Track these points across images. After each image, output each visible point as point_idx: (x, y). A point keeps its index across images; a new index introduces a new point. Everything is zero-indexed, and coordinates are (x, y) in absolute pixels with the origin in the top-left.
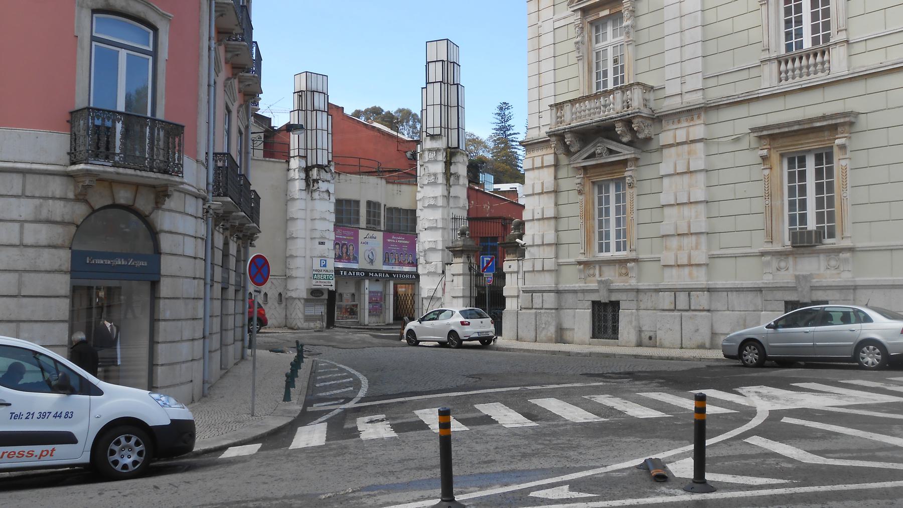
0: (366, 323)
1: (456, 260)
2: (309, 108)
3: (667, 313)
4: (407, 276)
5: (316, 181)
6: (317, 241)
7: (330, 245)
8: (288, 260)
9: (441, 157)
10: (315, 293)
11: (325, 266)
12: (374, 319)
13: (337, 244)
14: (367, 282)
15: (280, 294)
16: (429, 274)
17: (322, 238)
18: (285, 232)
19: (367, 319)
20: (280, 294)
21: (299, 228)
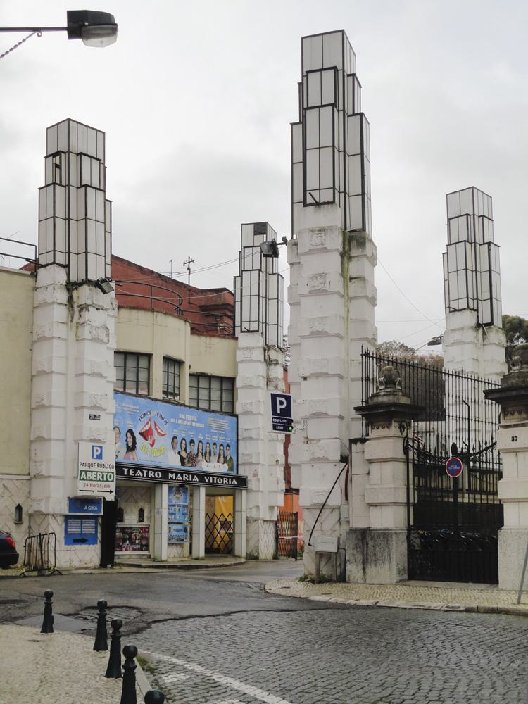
0: (164, 558)
1: (374, 433)
2: (73, 182)
3: (243, 609)
4: (225, 481)
5: (83, 308)
6: (87, 413)
7: (107, 422)
8: (34, 446)
9: (336, 242)
10: (78, 503)
11: (100, 457)
12: (175, 551)
13: (328, 361)
14: (165, 488)
15: (19, 508)
16: (315, 461)
17: (95, 407)
18: (29, 397)
19: (167, 553)
20: (19, 508)
21: (57, 390)
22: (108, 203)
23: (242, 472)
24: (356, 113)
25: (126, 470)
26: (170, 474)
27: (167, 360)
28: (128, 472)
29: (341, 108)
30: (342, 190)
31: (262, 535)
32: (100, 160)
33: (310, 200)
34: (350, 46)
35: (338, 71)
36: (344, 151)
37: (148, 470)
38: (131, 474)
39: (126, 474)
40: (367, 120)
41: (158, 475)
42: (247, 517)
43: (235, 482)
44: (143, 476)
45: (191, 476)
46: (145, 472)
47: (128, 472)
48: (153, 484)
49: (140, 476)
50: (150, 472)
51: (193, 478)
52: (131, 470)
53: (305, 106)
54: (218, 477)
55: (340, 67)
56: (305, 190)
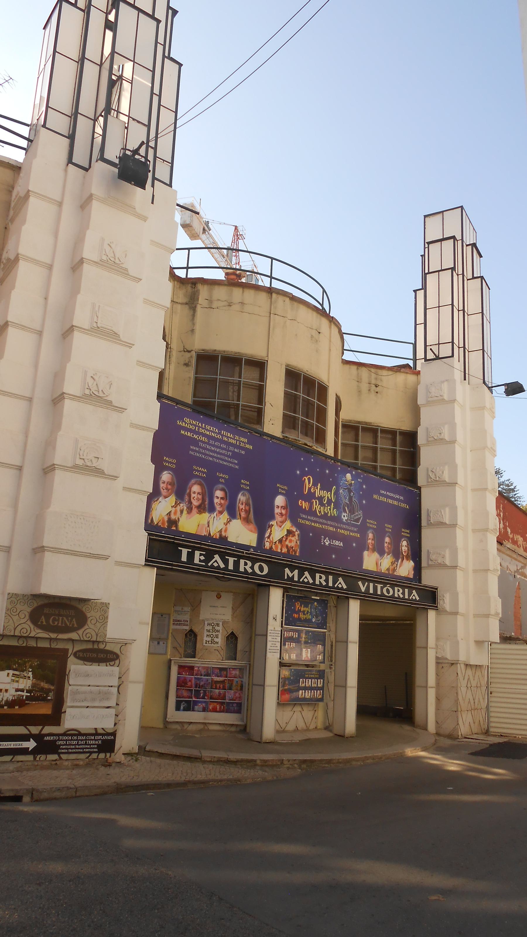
22: (170, 67)
23: (429, 578)
24: (475, 276)
25: (185, 552)
26: (287, 570)
27: (293, 376)
28: (191, 556)
29: (460, 272)
30: (461, 345)
31: (464, 689)
32: (158, 21)
33: (430, 356)
34: (470, 222)
35: (457, 241)
36: (464, 310)
37: (240, 557)
38: (196, 561)
39: (184, 558)
40: (487, 284)
41: (261, 569)
42: (437, 658)
43: (415, 596)
44: (226, 568)
45: (406, 590)
46: (231, 560)
47: (191, 556)
48: (256, 588)
49: (218, 567)
50: (242, 562)
51: (410, 594)
52: (197, 553)
53: (427, 271)
54: (385, 584)
55: (459, 237)
56: (426, 346)
